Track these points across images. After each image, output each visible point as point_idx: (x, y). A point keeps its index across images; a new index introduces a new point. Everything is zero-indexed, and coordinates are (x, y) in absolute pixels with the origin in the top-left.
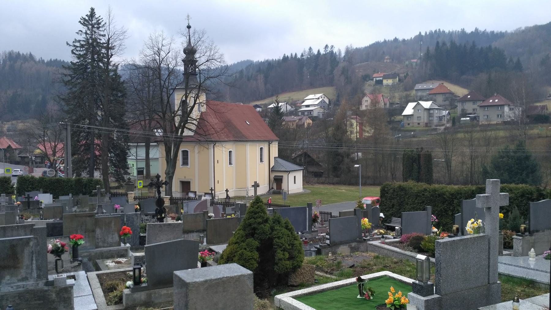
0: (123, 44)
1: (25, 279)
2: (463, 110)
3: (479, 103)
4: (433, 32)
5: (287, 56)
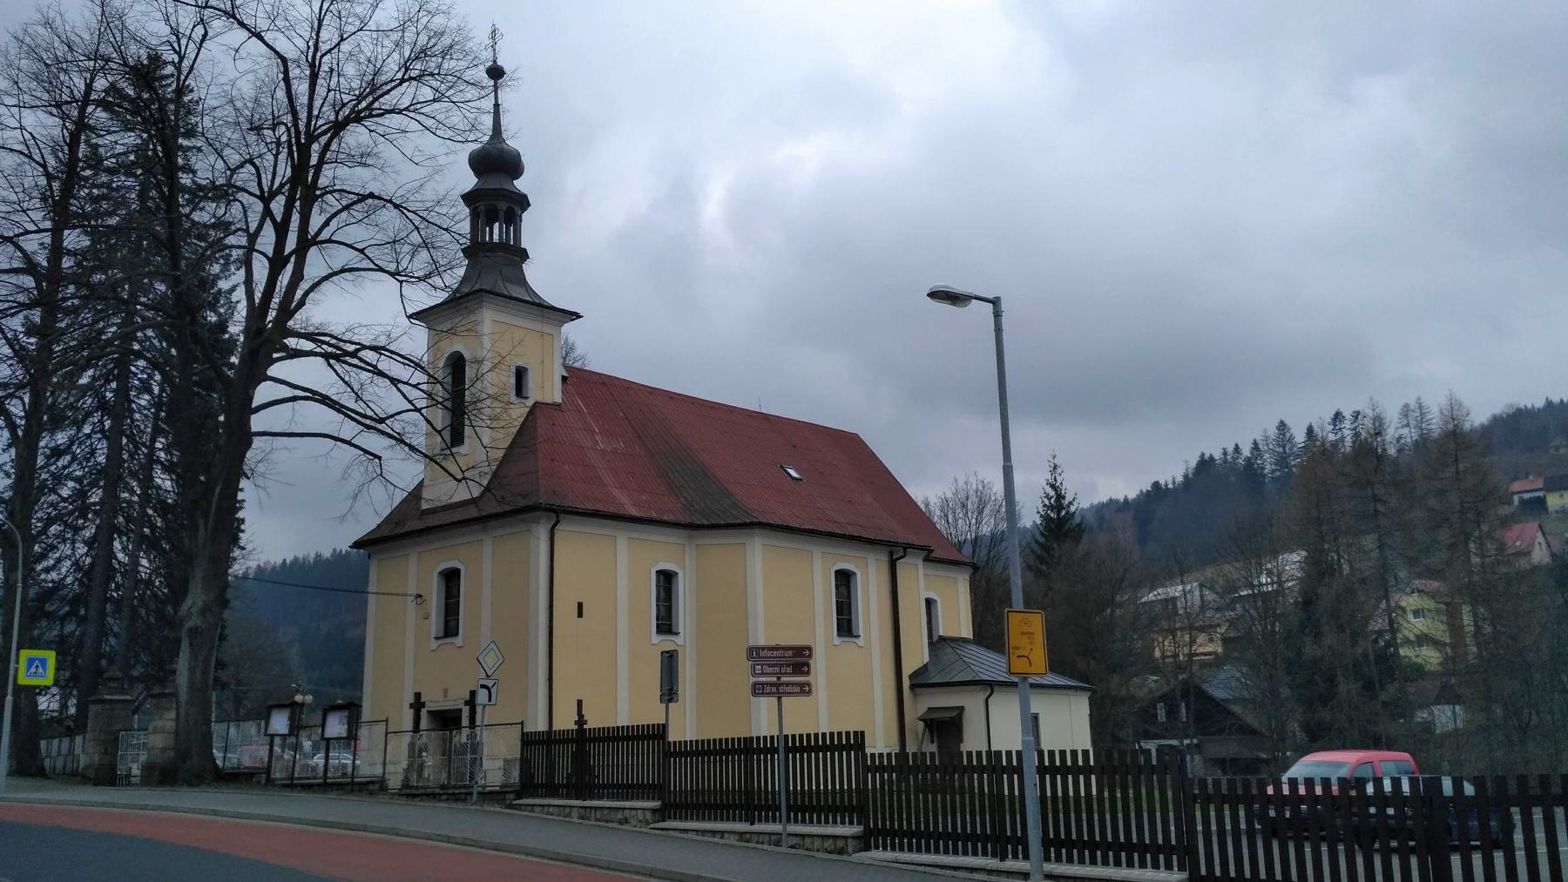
5: (1211, 457)
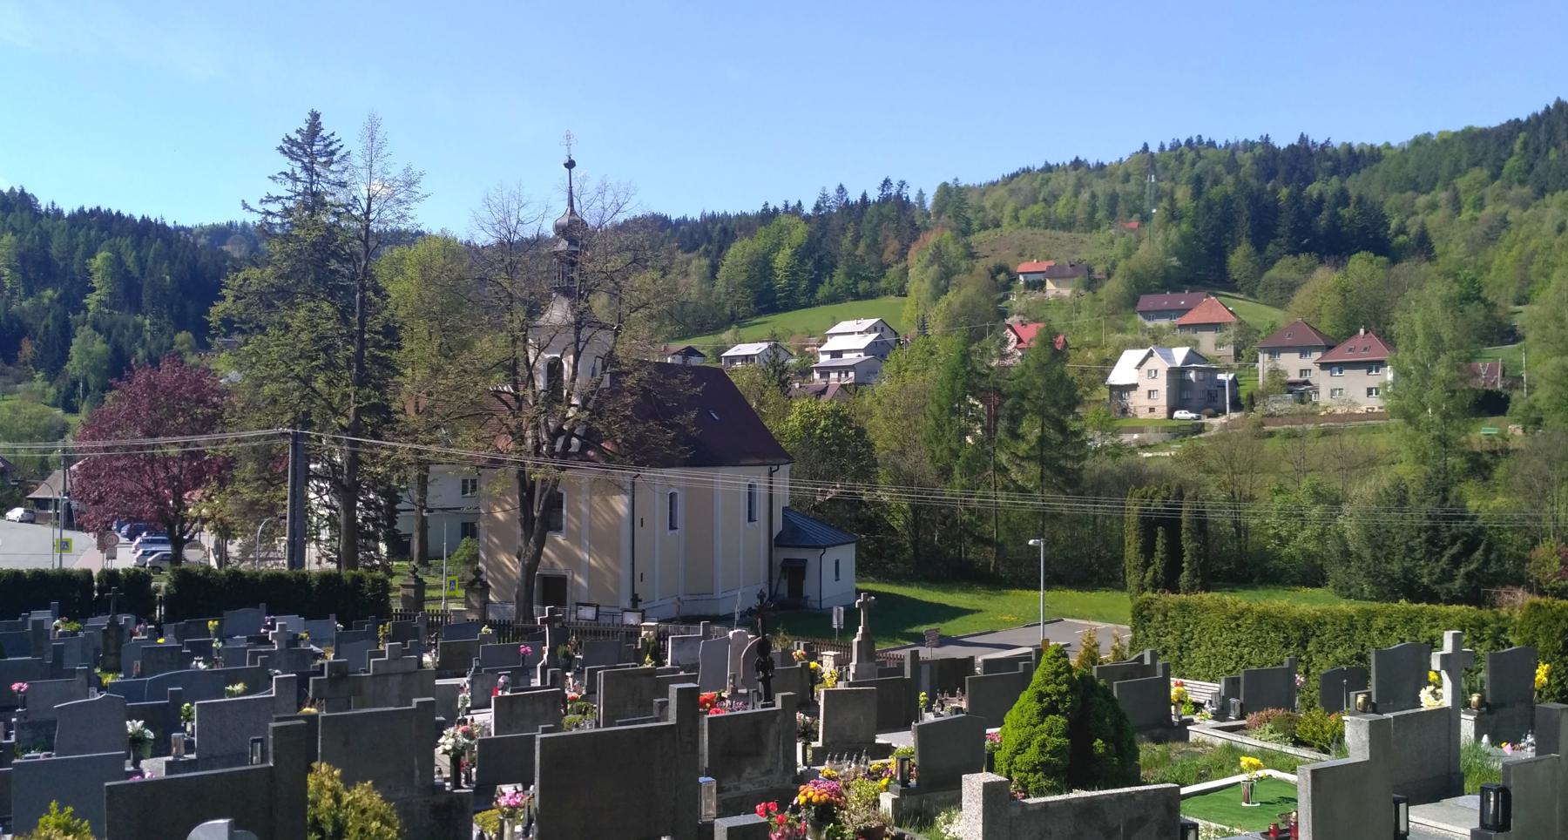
0: (411, 213)
1: (769, 772)
2: (1274, 372)
3: (1317, 355)
4: (1183, 142)
